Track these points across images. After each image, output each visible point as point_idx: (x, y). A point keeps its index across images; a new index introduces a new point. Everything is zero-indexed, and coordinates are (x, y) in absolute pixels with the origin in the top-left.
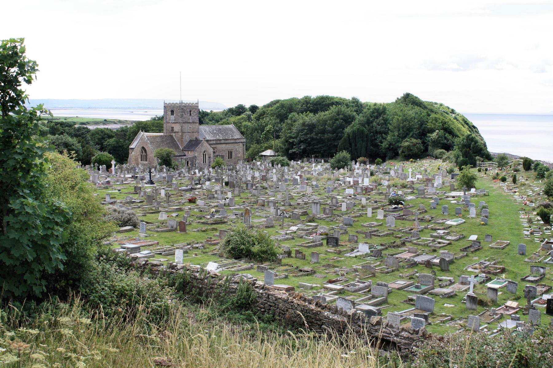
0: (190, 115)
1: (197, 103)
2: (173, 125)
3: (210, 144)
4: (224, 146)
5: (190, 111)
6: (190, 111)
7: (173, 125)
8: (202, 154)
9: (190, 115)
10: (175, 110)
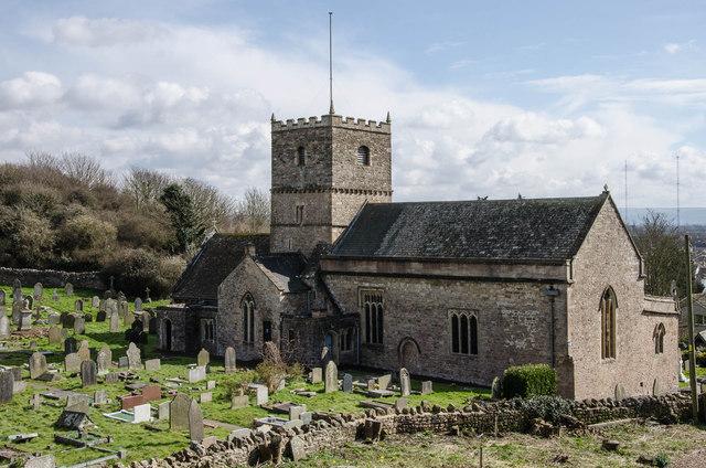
0: (301, 162)
4: (422, 287)
6: (301, 149)
9: (301, 162)
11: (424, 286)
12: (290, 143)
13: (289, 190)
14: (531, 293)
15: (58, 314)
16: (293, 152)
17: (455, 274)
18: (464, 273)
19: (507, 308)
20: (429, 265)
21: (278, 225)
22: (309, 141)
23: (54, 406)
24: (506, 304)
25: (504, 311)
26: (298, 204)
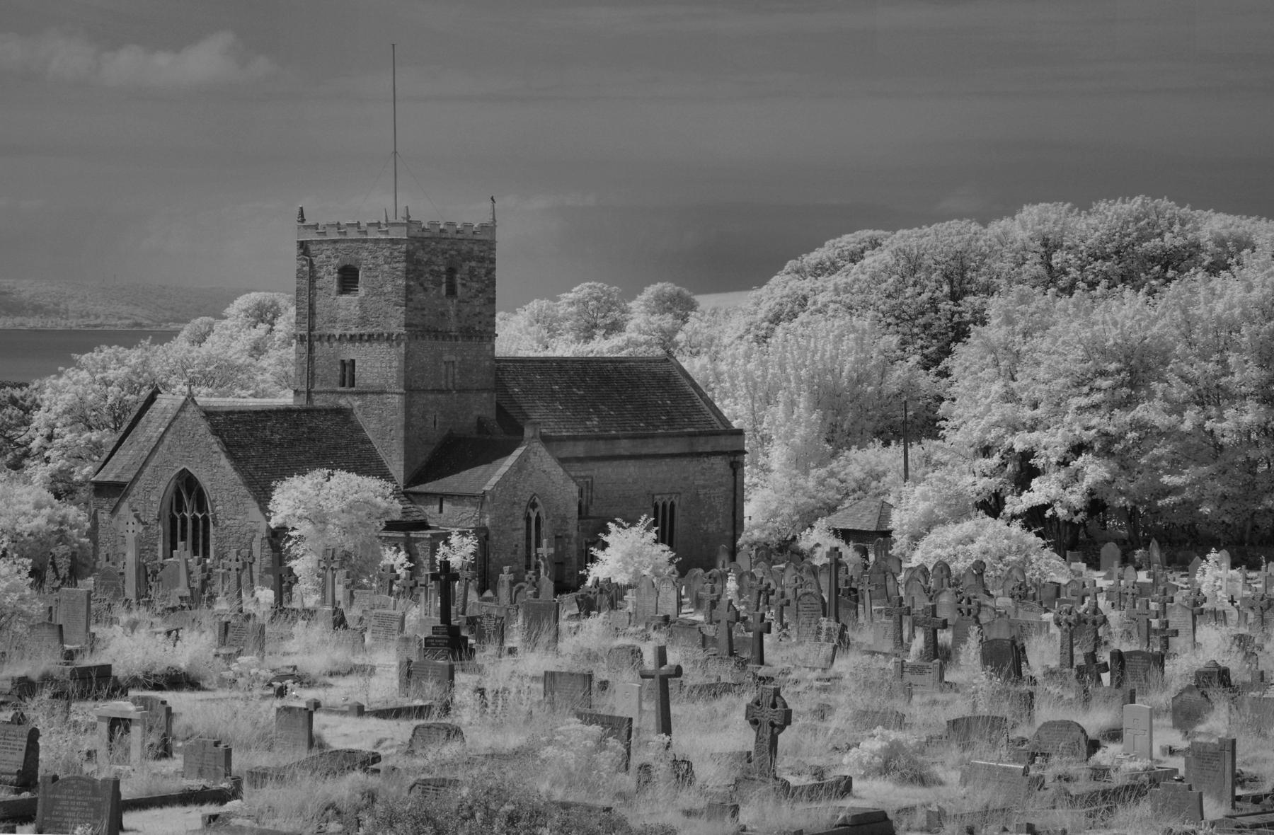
0: (451, 291)
1: (490, 228)
2: (350, 352)
3: (563, 461)
4: (631, 470)
5: (451, 271)
6: (451, 271)
7: (350, 352)
8: (519, 513)
9: (451, 291)
10: (364, 257)
11: (632, 469)
12: (434, 259)
13: (437, 334)
14: (720, 464)
15: (884, 243)
16: (439, 274)
17: (661, 452)
18: (714, 417)
19: (704, 487)
20: (639, 442)
21: (419, 390)
22: (464, 261)
23: (538, 518)
24: (702, 482)
25: (702, 491)
26: (446, 358)
